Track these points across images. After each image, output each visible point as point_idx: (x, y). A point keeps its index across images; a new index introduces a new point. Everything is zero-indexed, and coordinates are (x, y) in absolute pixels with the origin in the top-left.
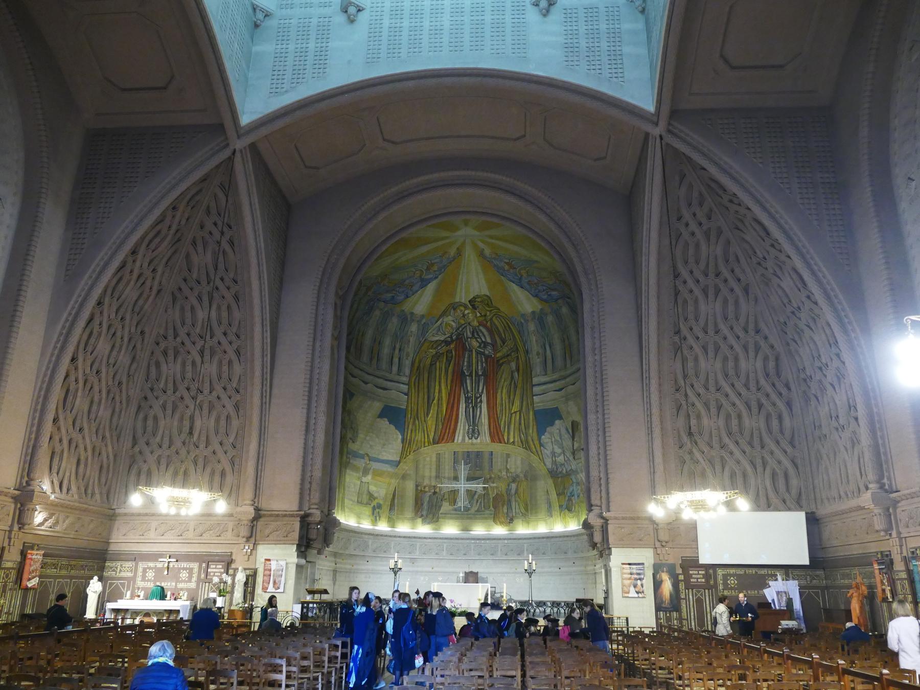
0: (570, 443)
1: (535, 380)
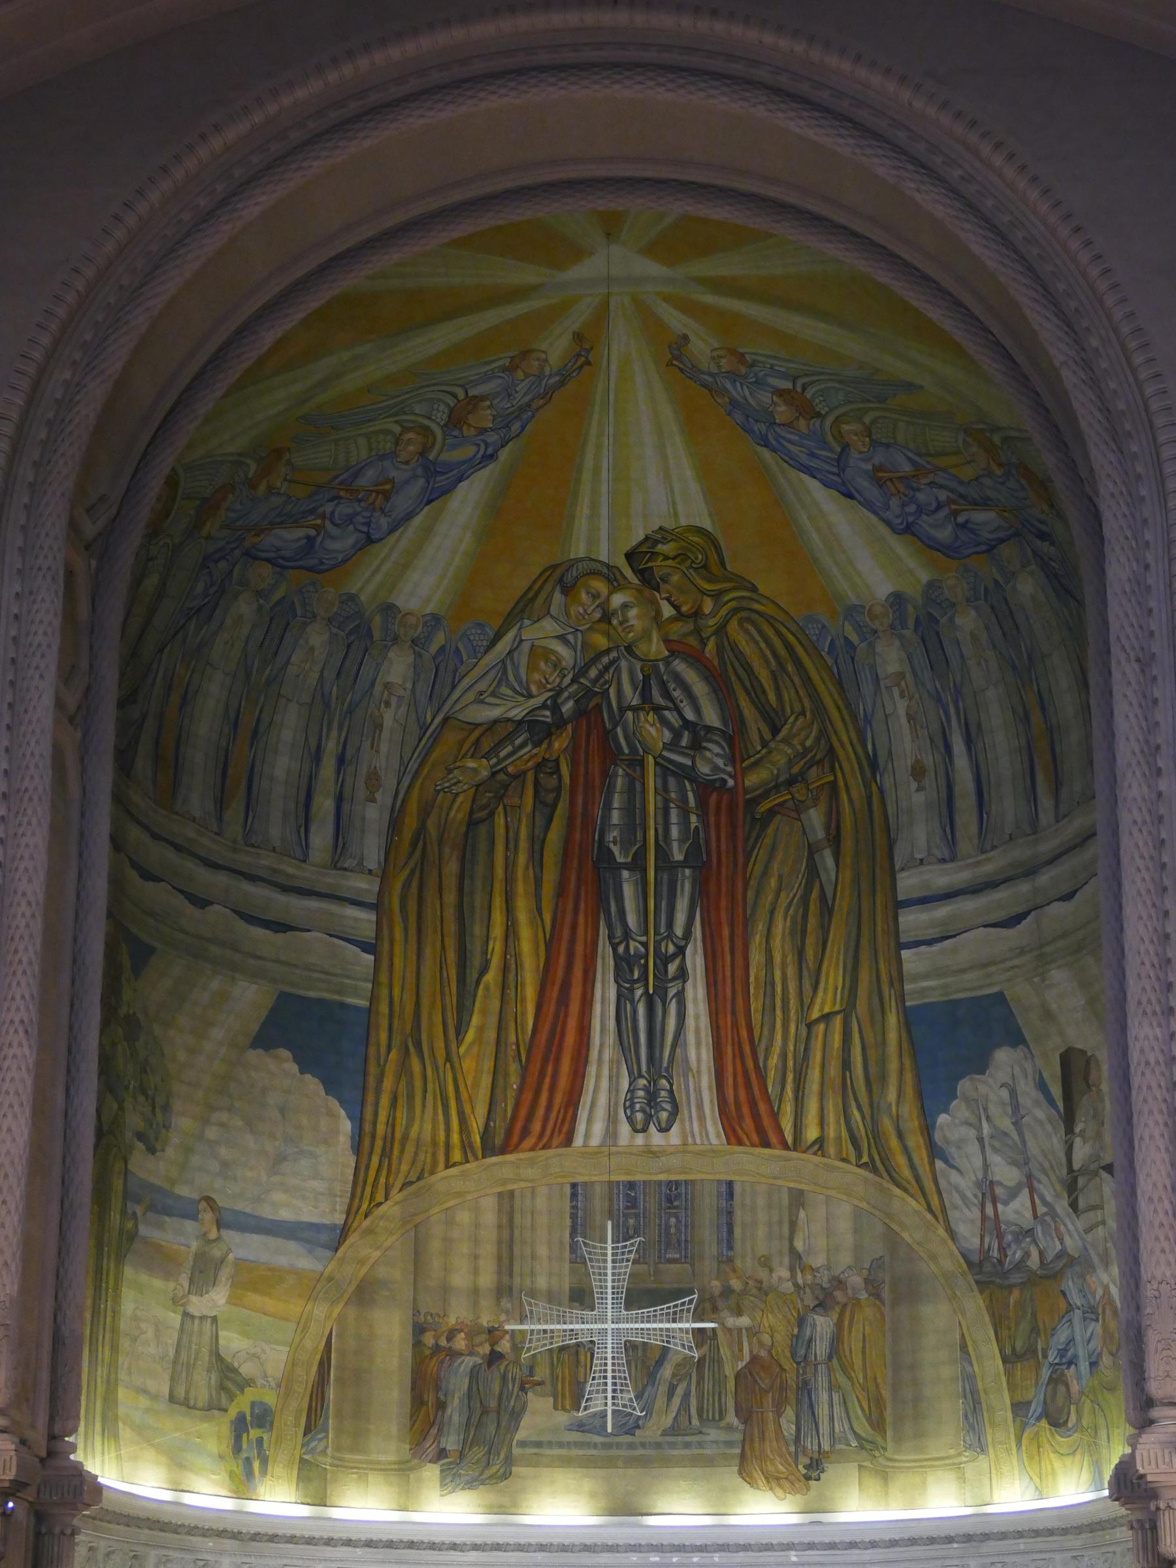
0: (1056, 1143)
1: (908, 883)
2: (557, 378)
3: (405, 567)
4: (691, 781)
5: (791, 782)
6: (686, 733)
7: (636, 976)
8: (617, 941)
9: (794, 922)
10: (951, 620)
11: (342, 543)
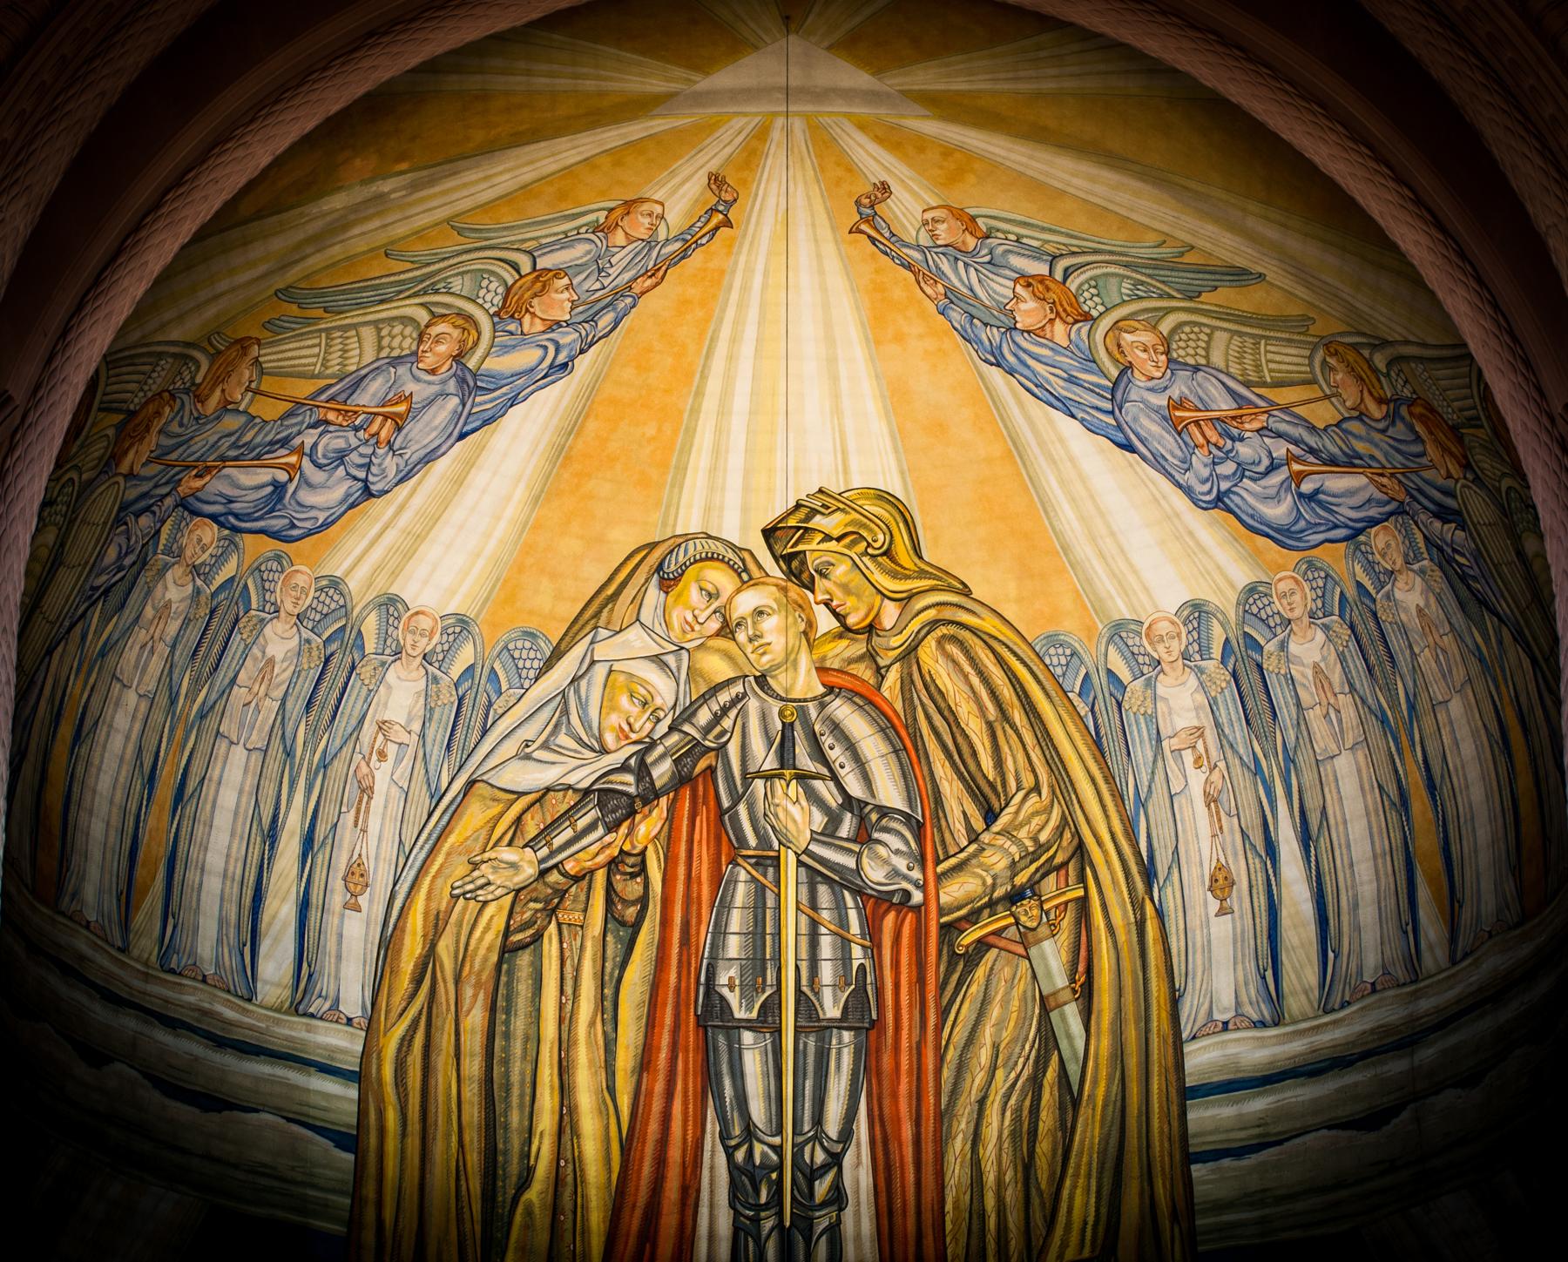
2: (678, 245)
3: (418, 538)
4: (858, 892)
5: (1015, 897)
6: (849, 815)
7: (763, 1199)
8: (733, 1143)
9: (1017, 1119)
10: (1283, 646)
11: (329, 492)
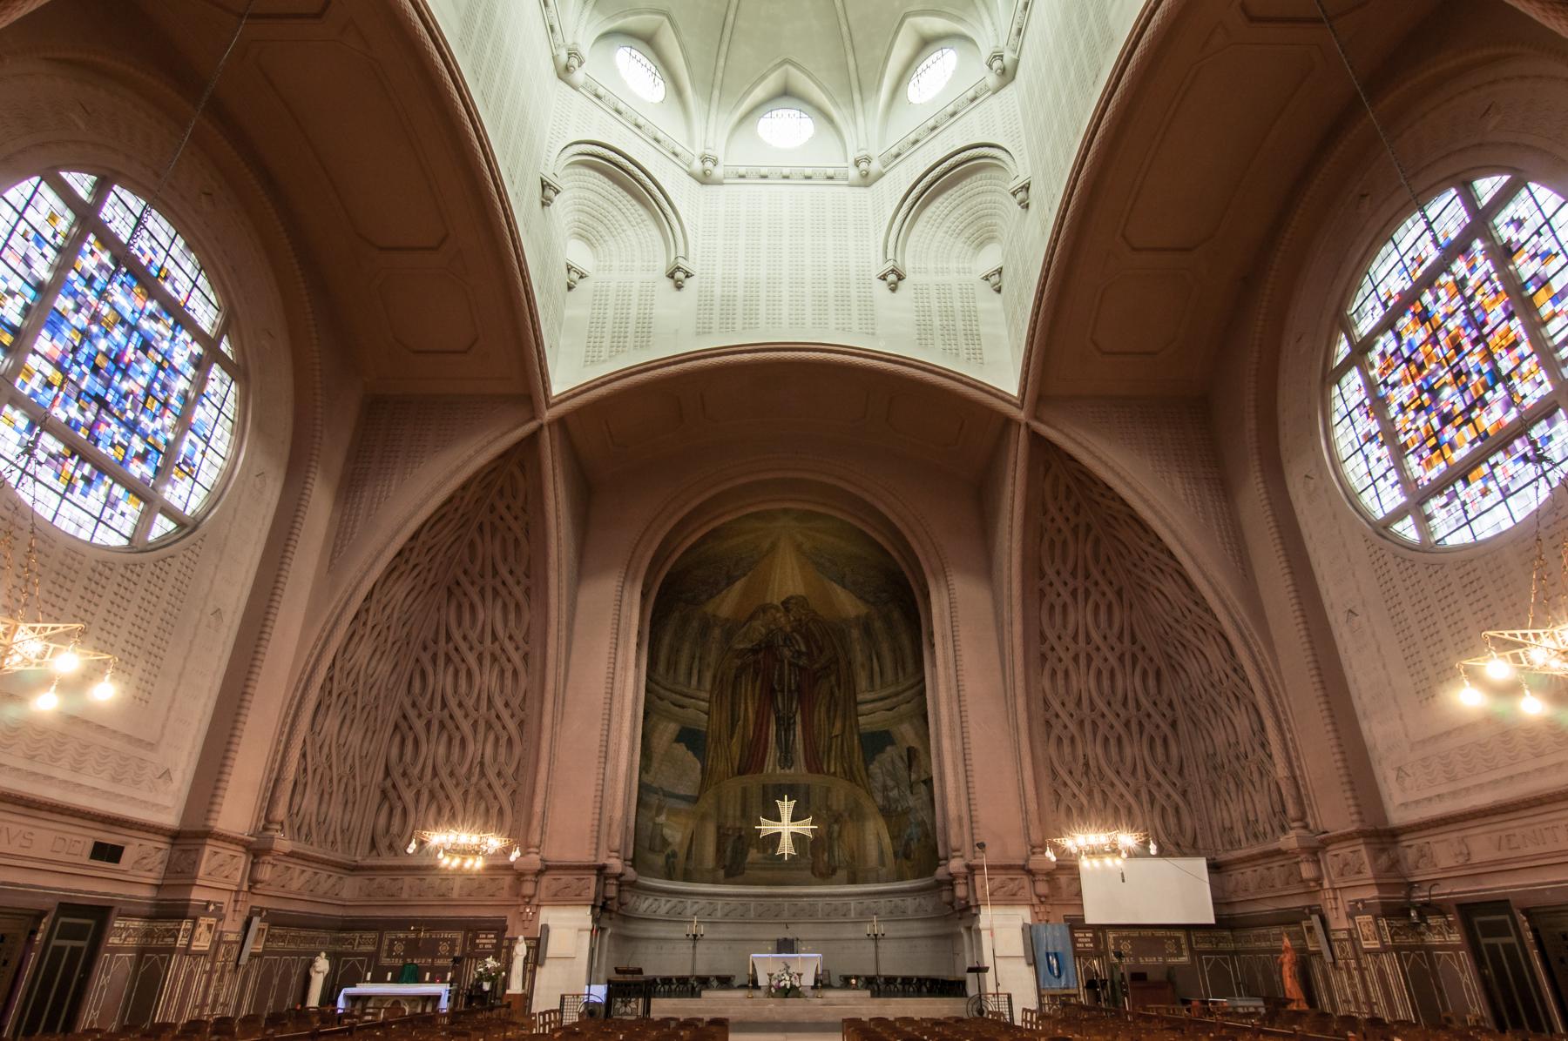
0: (905, 774)
1: (860, 697)
